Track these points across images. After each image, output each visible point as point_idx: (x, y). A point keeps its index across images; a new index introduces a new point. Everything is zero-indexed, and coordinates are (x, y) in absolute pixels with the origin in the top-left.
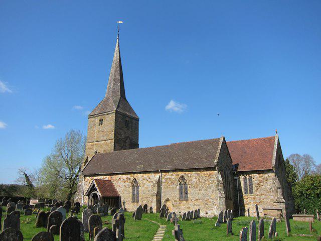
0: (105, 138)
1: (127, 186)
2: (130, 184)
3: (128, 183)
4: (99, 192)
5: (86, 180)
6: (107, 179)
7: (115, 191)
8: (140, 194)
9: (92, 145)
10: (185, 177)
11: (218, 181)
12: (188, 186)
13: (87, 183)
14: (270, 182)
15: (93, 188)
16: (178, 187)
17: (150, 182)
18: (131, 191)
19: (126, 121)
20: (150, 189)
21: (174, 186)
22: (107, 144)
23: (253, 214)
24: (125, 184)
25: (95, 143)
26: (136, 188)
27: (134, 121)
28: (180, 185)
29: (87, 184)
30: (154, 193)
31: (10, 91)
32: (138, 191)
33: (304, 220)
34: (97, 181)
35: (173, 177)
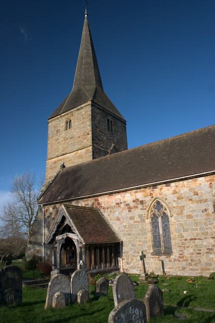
0: (76, 147)
3: (137, 212)
4: (76, 232)
7: (112, 233)
8: (174, 234)
15: (63, 228)
18: (149, 227)
23: (122, 271)
26: (160, 220)
31: (79, 300)
32: (166, 228)
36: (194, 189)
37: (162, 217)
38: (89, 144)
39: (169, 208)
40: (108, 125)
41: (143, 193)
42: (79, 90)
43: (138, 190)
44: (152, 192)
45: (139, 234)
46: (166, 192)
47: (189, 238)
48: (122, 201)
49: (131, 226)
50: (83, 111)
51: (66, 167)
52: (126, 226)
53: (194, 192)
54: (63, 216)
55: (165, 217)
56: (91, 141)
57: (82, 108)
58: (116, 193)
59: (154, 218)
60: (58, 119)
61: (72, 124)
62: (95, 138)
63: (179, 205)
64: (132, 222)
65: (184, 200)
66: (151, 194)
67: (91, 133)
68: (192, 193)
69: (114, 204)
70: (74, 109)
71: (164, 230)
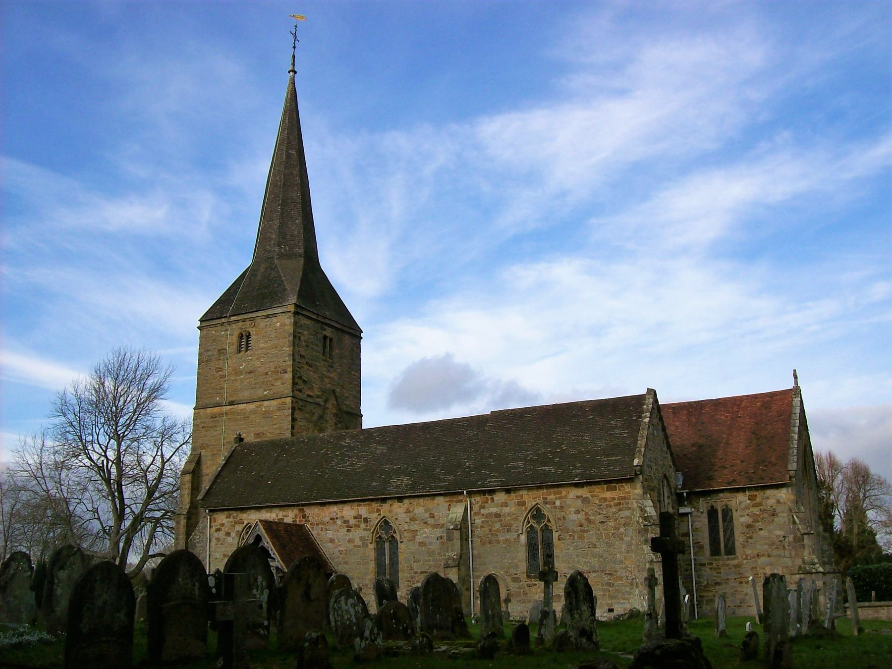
1: (358, 542)
2: (367, 535)
3: (357, 534)
5: (216, 525)
6: (288, 520)
8: (403, 565)
9: (213, 417)
10: (546, 510)
11: (646, 518)
12: (555, 535)
13: (221, 535)
14: (783, 517)
16: (523, 538)
17: (436, 526)
18: (372, 554)
19: (325, 337)
20: (435, 546)
21: (512, 536)
22: (267, 415)
24: (350, 535)
25: (225, 409)
26: (387, 545)
27: (347, 340)
28: (528, 532)
29: (218, 539)
30: (449, 558)
33: (876, 615)
34: (267, 524)
35: (506, 510)
36: (430, 510)
37: (390, 541)
38: (286, 392)
39: (400, 531)
40: (324, 347)
41: (367, 508)
42: (303, 410)
43: (362, 503)
44: (379, 508)
45: (359, 564)
46: (397, 512)
47: (419, 571)
48: (338, 516)
49: (348, 552)
50: (277, 322)
51: (245, 441)
52: (342, 551)
53: (431, 514)
54: (258, 535)
55: (393, 541)
56: (290, 387)
57: (274, 315)
58: (330, 503)
59: (380, 541)
60: (222, 324)
61: (252, 342)
62: (297, 380)
63: (412, 528)
64: (351, 546)
65: (417, 522)
66: (378, 510)
67: (290, 369)
68: (427, 515)
69: (327, 519)
70: (259, 314)
71: (391, 559)
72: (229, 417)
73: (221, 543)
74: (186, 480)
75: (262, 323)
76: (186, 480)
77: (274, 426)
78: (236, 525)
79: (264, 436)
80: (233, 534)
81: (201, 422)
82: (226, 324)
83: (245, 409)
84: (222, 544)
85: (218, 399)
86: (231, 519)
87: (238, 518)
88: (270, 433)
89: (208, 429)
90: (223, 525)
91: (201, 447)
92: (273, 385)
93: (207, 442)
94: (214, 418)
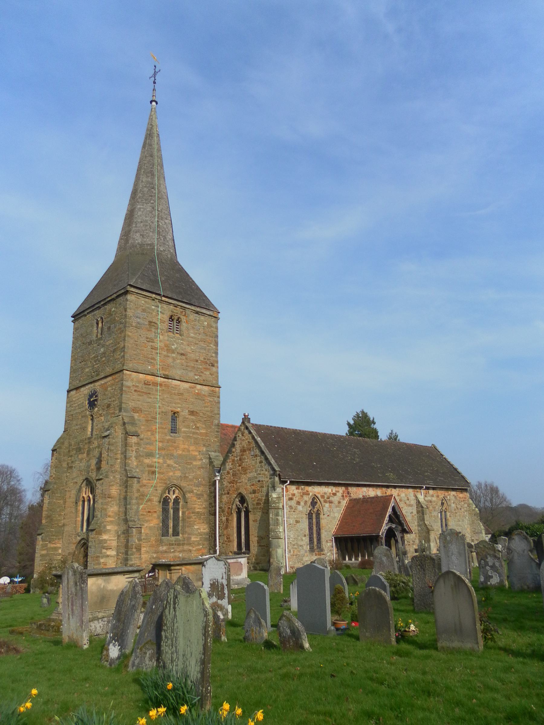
9: (146, 383)
13: (293, 503)
22: (199, 396)
25: (159, 380)
29: (291, 507)
72: (163, 388)
73: (293, 510)
74: (133, 442)
75: (193, 316)
76: (133, 442)
77: (206, 409)
78: (304, 496)
79: (198, 415)
80: (302, 503)
81: (133, 385)
82: (157, 300)
83: (179, 386)
84: (294, 511)
85: (149, 367)
86: (300, 491)
87: (305, 490)
88: (203, 413)
89: (141, 394)
90: (294, 495)
91: (133, 410)
92: (202, 373)
93: (141, 407)
94: (147, 384)
